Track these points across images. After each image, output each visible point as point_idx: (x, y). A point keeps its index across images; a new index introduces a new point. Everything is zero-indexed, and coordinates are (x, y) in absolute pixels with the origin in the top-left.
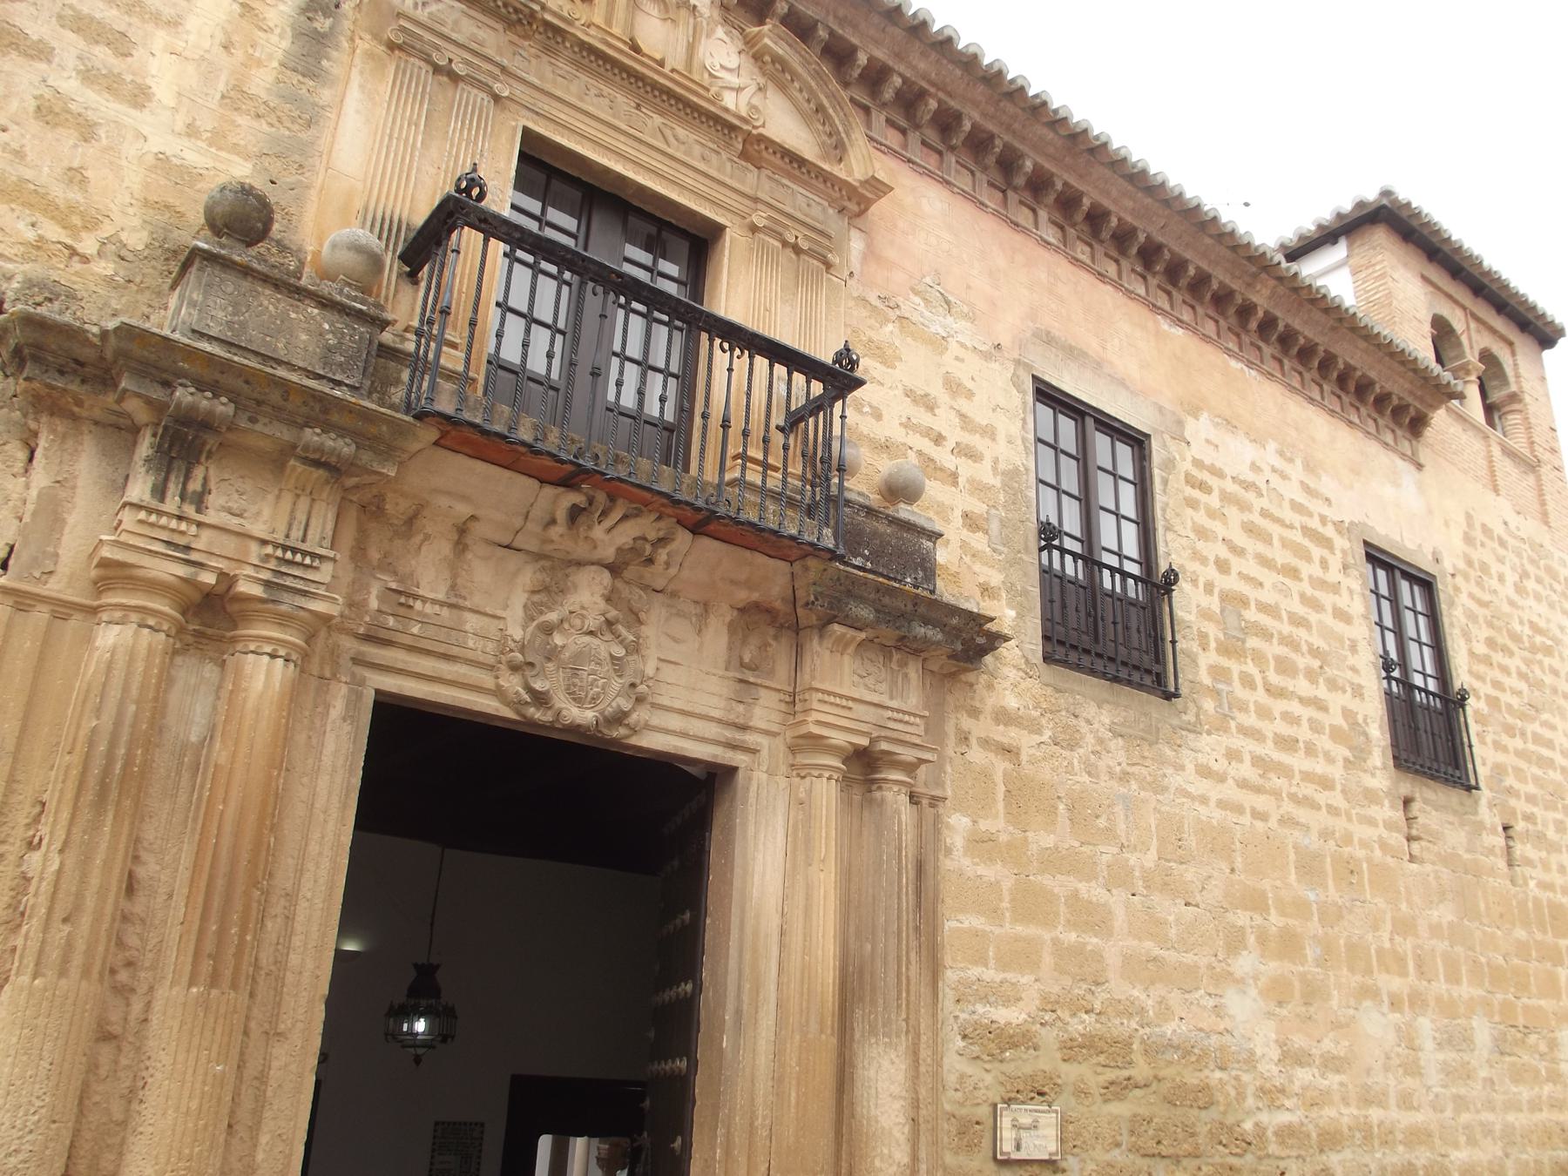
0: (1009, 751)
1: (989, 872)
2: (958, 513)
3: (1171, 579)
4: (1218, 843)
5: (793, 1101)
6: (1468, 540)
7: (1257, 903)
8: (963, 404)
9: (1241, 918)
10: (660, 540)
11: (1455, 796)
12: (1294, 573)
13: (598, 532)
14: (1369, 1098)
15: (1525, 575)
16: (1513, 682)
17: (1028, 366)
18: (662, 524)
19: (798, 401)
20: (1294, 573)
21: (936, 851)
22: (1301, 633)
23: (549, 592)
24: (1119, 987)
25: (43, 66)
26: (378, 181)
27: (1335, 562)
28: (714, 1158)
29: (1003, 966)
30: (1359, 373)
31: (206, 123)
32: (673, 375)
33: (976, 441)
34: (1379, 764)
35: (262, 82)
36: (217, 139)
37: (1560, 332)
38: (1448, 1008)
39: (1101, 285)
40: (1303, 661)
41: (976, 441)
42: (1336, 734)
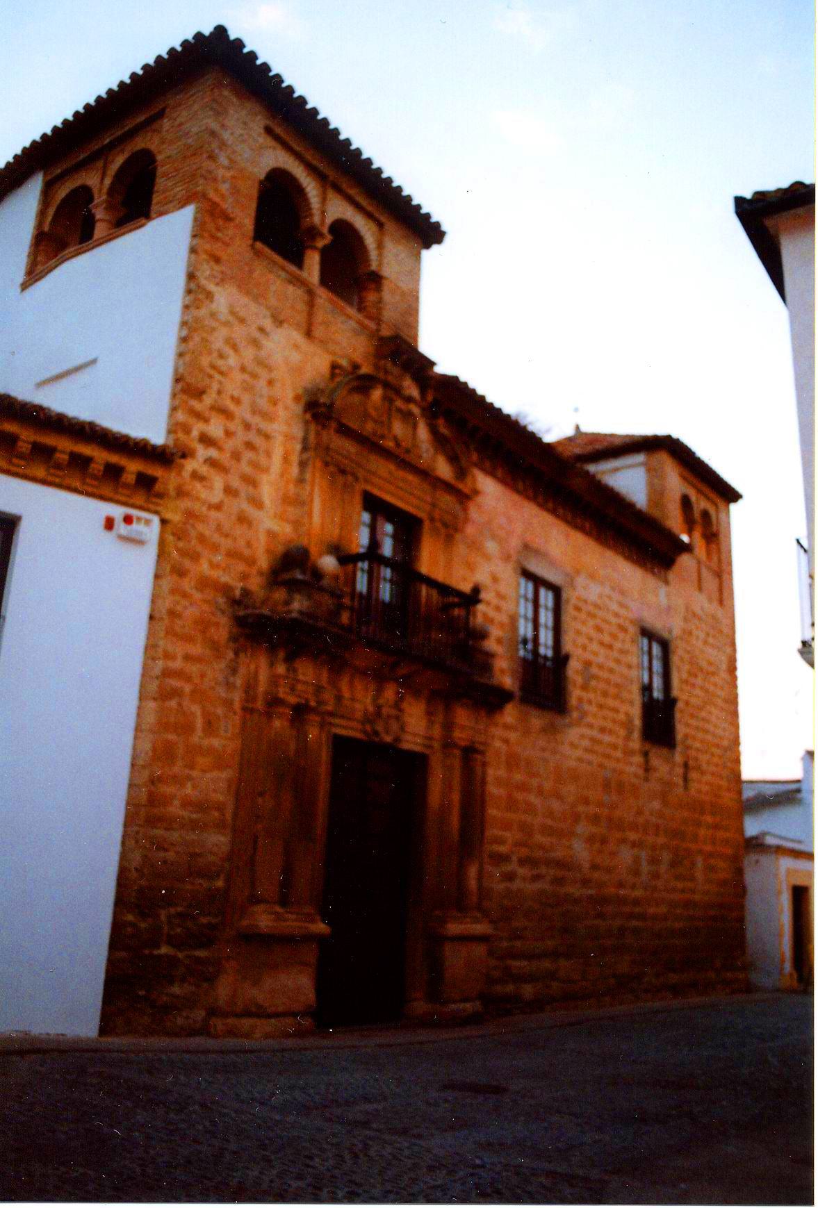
3: (567, 658)
4: (575, 777)
7: (586, 802)
9: (581, 808)
11: (665, 751)
12: (610, 647)
14: (621, 885)
15: (708, 634)
16: (698, 691)
20: (610, 647)
22: (611, 677)
23: (380, 690)
24: (539, 838)
27: (628, 638)
39: (750, 889)
40: (612, 691)
42: (623, 724)
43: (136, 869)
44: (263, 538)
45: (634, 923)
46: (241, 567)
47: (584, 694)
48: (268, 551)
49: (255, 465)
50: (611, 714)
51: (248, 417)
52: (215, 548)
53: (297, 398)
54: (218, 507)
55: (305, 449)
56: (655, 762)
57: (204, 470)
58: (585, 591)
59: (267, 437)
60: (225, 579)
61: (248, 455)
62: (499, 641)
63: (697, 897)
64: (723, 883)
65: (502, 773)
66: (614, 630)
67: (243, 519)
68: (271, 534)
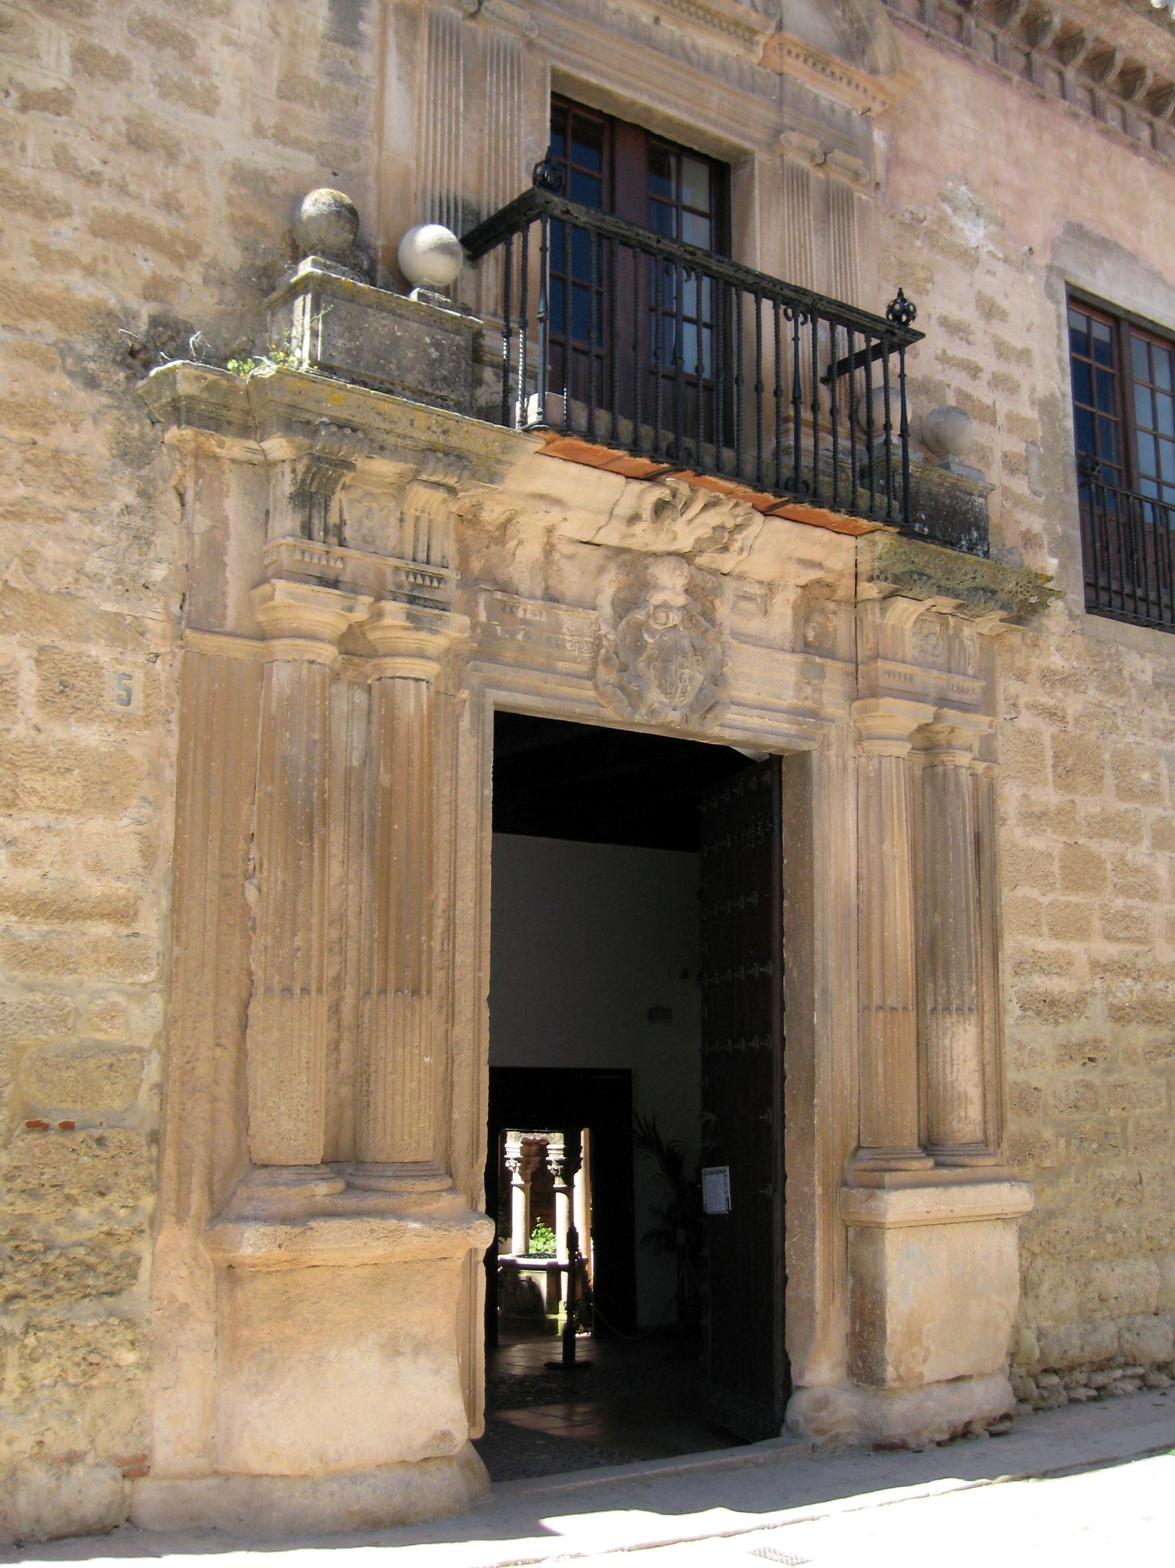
0: (1052, 715)
1: (1038, 843)
2: (998, 455)
5: (880, 1071)
8: (997, 328)
10: (737, 526)
13: (680, 525)
17: (1061, 272)
18: (739, 510)
19: (843, 353)
21: (992, 822)
25: (126, 84)
26: (431, 158)
28: (812, 1125)
29: (1056, 934)
31: (270, 120)
32: (689, 320)
33: (1014, 370)
35: (311, 64)
36: (281, 136)
41: (1014, 370)
43: (402, 1354)
44: (219, 189)
46: (149, 264)
60: (87, 290)
62: (1011, 465)
65: (1050, 797)
68: (242, 175)
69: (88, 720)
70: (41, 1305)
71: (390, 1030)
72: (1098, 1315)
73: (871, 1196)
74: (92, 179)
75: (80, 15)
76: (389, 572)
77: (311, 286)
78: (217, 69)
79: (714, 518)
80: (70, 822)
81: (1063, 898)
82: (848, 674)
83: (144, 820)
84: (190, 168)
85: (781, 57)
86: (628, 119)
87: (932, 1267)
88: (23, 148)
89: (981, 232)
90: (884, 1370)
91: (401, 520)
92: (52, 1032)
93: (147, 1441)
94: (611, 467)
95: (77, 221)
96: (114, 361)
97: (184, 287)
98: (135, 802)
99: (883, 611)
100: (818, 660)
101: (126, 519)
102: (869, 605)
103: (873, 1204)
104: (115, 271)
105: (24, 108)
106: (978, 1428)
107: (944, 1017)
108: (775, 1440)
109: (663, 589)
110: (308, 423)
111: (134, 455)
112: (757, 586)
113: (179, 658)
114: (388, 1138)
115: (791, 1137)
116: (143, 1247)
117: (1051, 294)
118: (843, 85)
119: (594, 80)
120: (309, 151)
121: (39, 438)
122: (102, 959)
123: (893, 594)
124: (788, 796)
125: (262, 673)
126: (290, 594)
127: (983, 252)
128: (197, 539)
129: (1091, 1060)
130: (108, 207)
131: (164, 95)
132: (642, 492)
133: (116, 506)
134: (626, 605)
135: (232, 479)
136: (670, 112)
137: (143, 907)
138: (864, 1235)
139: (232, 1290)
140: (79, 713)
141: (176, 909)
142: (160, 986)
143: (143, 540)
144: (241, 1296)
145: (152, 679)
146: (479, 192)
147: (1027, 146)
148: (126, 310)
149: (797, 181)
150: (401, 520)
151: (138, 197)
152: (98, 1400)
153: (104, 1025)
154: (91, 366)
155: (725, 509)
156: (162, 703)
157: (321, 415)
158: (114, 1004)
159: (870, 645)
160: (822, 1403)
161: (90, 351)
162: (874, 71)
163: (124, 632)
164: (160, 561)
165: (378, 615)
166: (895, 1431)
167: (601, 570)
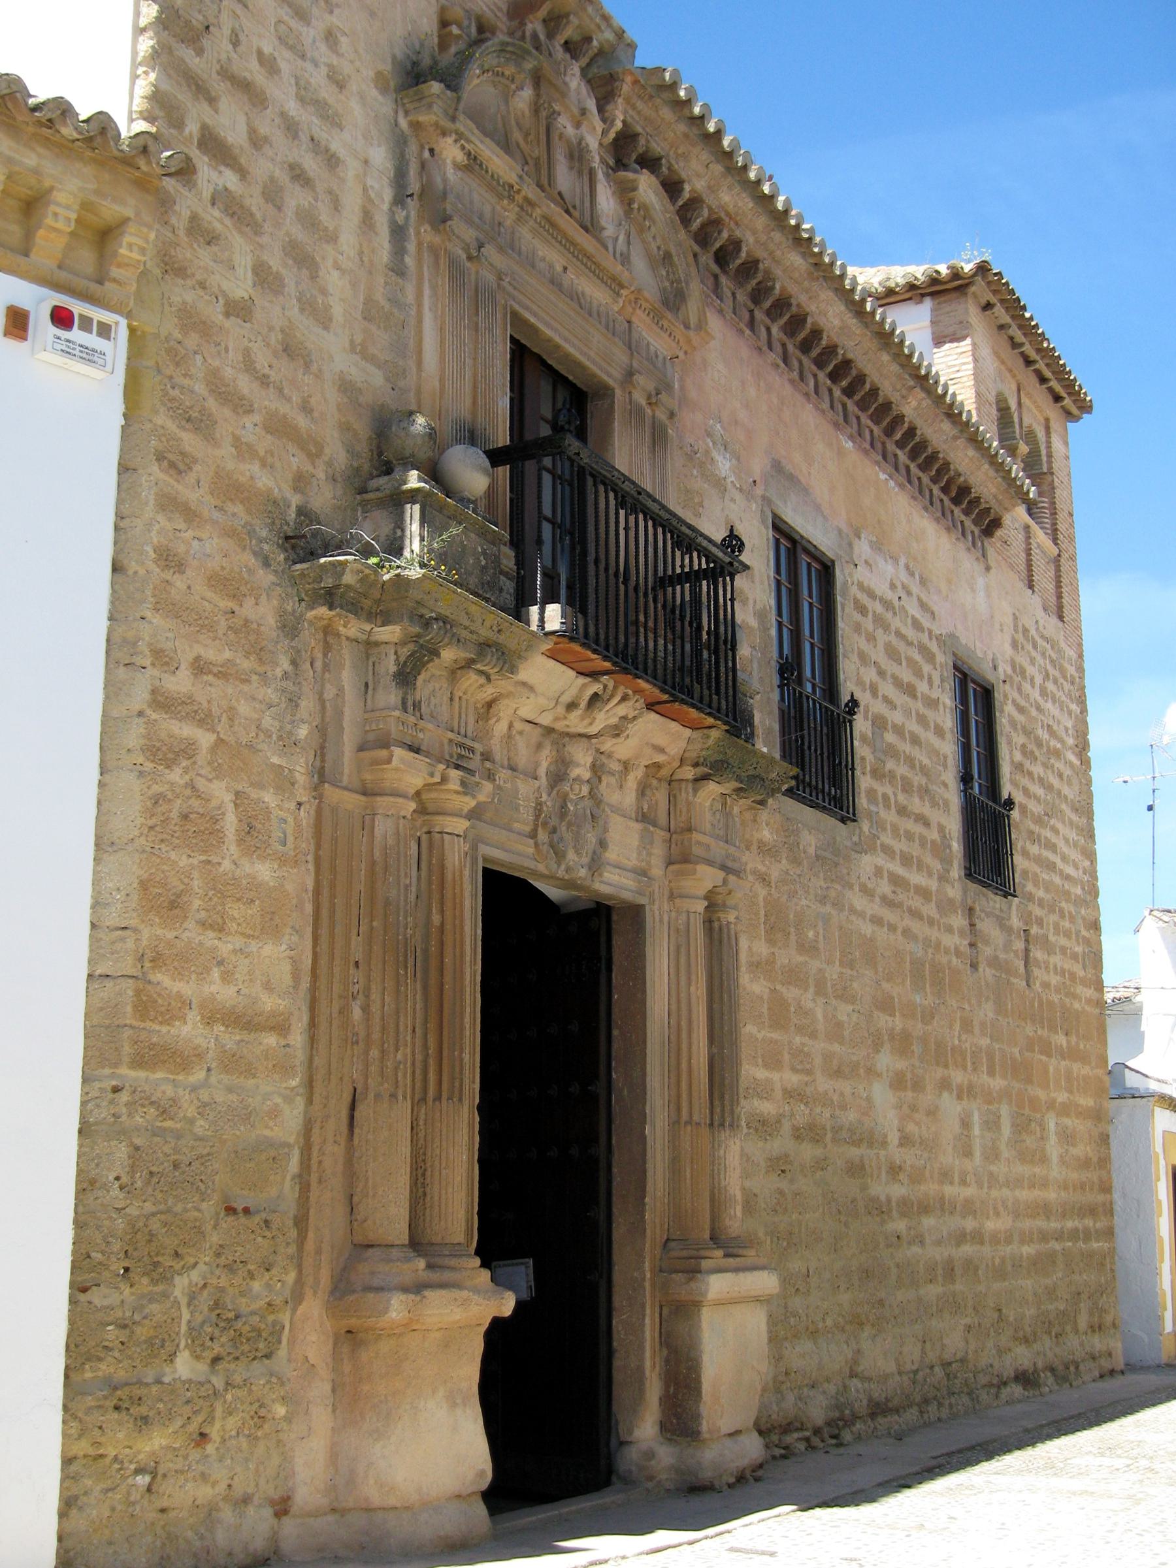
6: (1015, 644)
29: (766, 1066)
30: (962, 479)
34: (957, 877)
37: (1086, 407)
38: (990, 1098)
45: (967, 1249)
46: (297, 461)
47: (876, 785)
48: (345, 428)
49: (308, 219)
50: (917, 829)
51: (293, 107)
52: (240, 405)
53: (380, 80)
54: (239, 310)
55: (401, 198)
56: (986, 926)
57: (214, 218)
58: (865, 576)
59: (332, 161)
60: (264, 481)
61: (296, 198)
63: (1051, 1195)
64: (1086, 1164)
65: (762, 949)
66: (226, 421)
67: (290, 349)
68: (346, 387)
69: (263, 858)
70: (232, 1366)
71: (444, 1132)
72: (784, 1387)
73: (691, 1279)
74: (264, 381)
75: (256, 233)
76: (446, 741)
77: (419, 498)
78: (331, 291)
79: (622, 710)
80: (254, 946)
81: (769, 1035)
82: (664, 841)
83: (293, 946)
84: (317, 376)
85: (634, 309)
86: (535, 350)
87: (735, 1336)
88: (227, 350)
89: (728, 465)
90: (700, 1424)
91: (451, 699)
92: (242, 1128)
93: (290, 1484)
94: (573, 665)
95: (257, 418)
96: (278, 544)
97: (314, 481)
98: (289, 930)
99: (695, 791)
100: (652, 829)
101: (284, 684)
102: (683, 785)
103: (693, 1285)
104: (278, 464)
105: (227, 315)
106: (748, 1474)
107: (719, 1132)
108: (609, 1489)
109: (578, 765)
110: (422, 616)
111: (290, 628)
112: (617, 763)
113: (314, 807)
114: (442, 1223)
115: (618, 1233)
116: (285, 1318)
117: (763, 522)
118: (665, 336)
119: (532, 320)
120: (379, 367)
121: (236, 608)
122: (270, 1066)
123: (705, 778)
124: (617, 941)
125: (366, 822)
126: (402, 760)
127: (729, 480)
128: (328, 704)
129: (783, 1171)
130: (273, 407)
131: (302, 310)
132: (584, 686)
133: (279, 672)
134: (558, 777)
135: (347, 655)
136: (572, 350)
137: (294, 1021)
138: (680, 1313)
139: (353, 1350)
140: (258, 852)
141: (313, 1024)
142: (301, 1090)
143: (293, 702)
144: (364, 1356)
145: (298, 824)
146: (474, 413)
147: (752, 392)
148: (284, 499)
149: (636, 413)
150: (451, 699)
151: (289, 400)
152: (261, 1449)
153: (271, 1124)
154: (266, 547)
155: (630, 703)
156: (304, 845)
157: (432, 611)
158: (276, 1105)
159: (683, 818)
160: (650, 1455)
161: (264, 533)
162: (687, 327)
163: (283, 781)
164: (302, 721)
165: (444, 779)
166: (707, 1474)
167: (539, 746)
